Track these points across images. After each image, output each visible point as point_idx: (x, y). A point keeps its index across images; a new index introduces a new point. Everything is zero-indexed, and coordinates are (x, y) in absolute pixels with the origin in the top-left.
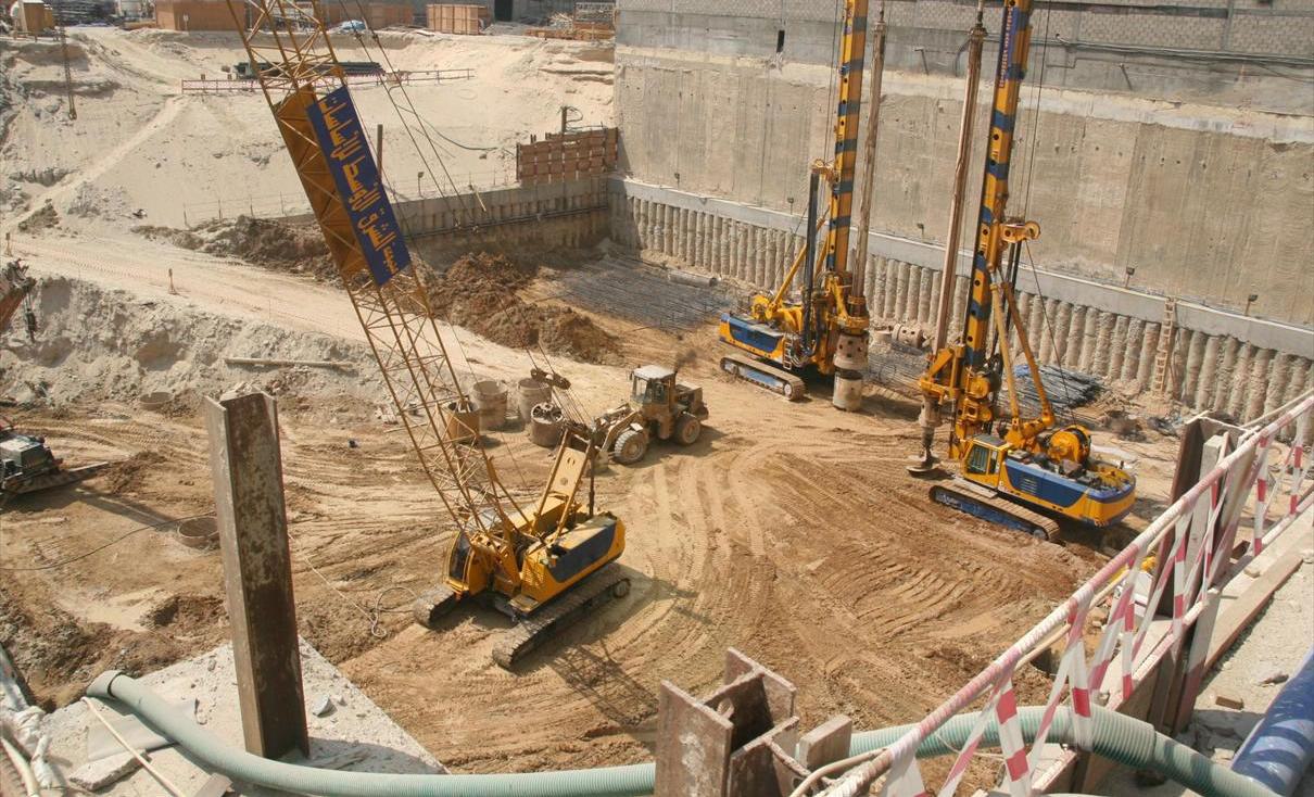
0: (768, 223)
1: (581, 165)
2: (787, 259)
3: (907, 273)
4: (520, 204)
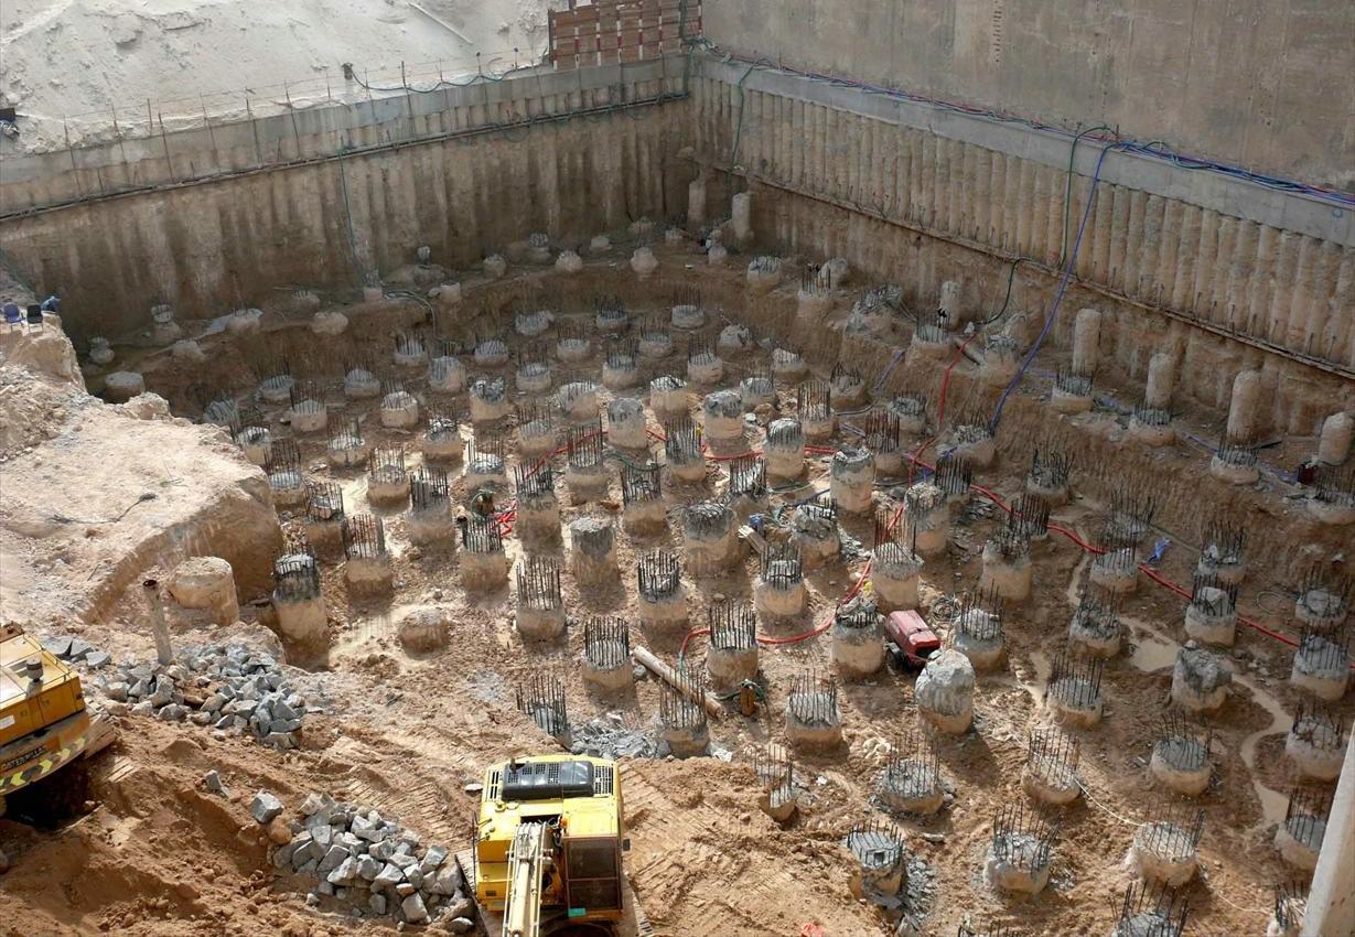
0: (898, 118)
1: (647, 37)
2: (926, 170)
3: (1094, 192)
4: (556, 96)
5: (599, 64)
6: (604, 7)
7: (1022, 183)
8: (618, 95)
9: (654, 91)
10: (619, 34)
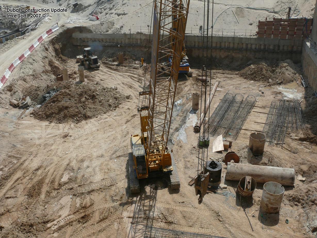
1: (290, 33)
5: (272, 38)
6: (276, 22)
7: (265, 64)
8: (277, 48)
9: (289, 49)
10: (280, 31)
